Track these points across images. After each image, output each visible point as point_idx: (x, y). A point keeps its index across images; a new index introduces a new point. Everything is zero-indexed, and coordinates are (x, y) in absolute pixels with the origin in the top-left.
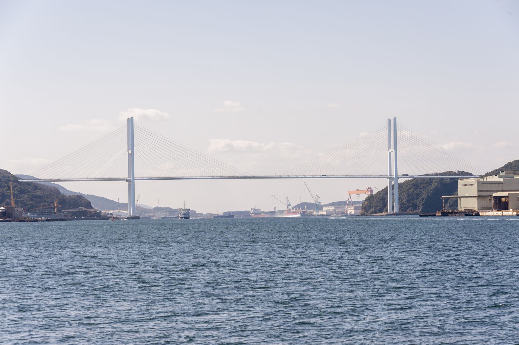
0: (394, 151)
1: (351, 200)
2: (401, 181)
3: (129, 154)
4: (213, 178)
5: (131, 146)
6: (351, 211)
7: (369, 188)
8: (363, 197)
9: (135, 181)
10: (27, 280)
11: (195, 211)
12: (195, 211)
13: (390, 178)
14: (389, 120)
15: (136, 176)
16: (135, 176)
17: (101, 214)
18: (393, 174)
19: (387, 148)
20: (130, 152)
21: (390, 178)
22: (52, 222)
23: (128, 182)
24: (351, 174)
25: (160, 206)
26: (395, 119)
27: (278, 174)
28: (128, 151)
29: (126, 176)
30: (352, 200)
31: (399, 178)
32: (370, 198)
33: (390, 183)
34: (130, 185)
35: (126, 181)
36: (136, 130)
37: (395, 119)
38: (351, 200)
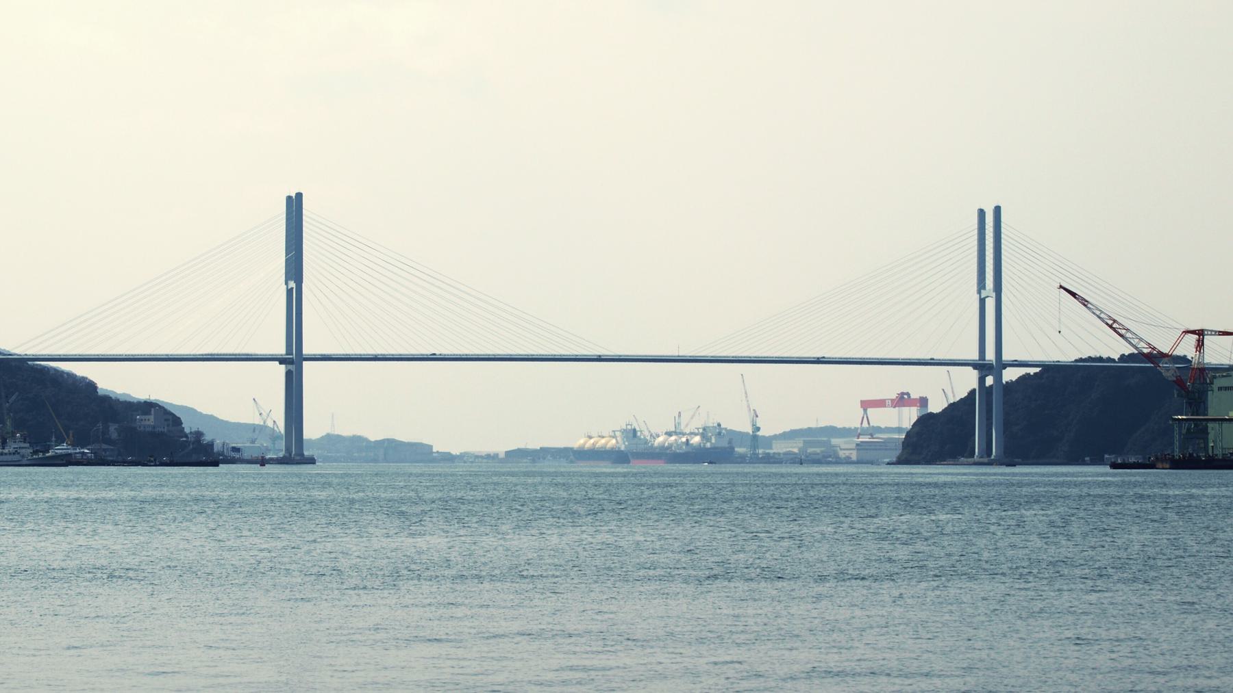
0: (994, 295)
1: (869, 423)
2: (1010, 375)
3: (289, 292)
4: (599, 359)
5: (294, 269)
6: (847, 453)
7: (903, 394)
8: (909, 417)
9: (304, 363)
10: (916, 615)
11: (431, 446)
12: (431, 446)
13: (982, 367)
14: (982, 213)
15: (306, 350)
16: (305, 352)
17: (212, 449)
18: (990, 355)
19: (975, 288)
20: (292, 284)
21: (982, 367)
22: (234, 466)
23: (283, 366)
24: (819, 355)
25: (336, 433)
26: (997, 210)
27: (926, 356)
28: (286, 283)
29: (281, 350)
30: (871, 425)
31: (1005, 368)
32: (926, 422)
33: (982, 380)
34: (289, 374)
35: (280, 364)
36: (1008, 260)
37: (997, 210)
38: (869, 423)
